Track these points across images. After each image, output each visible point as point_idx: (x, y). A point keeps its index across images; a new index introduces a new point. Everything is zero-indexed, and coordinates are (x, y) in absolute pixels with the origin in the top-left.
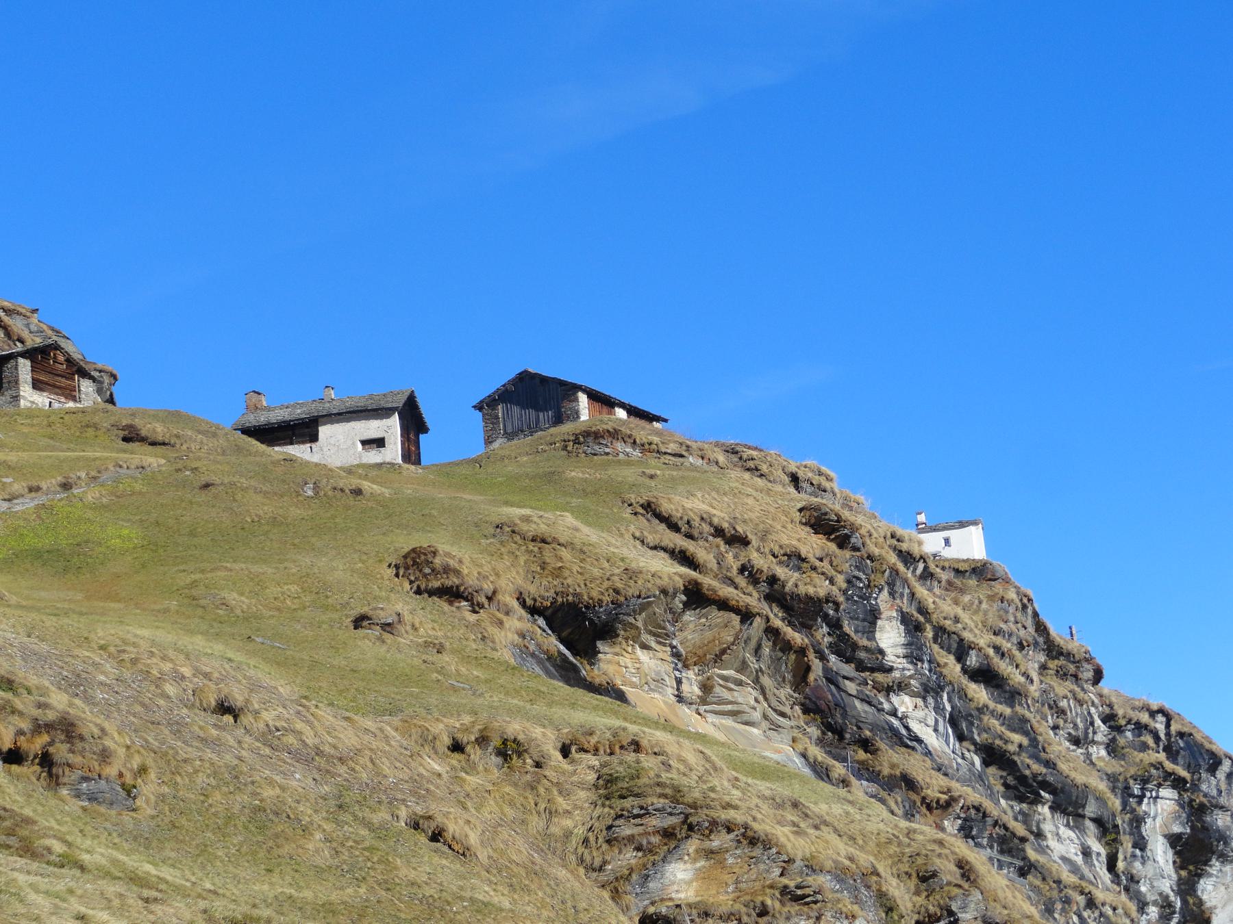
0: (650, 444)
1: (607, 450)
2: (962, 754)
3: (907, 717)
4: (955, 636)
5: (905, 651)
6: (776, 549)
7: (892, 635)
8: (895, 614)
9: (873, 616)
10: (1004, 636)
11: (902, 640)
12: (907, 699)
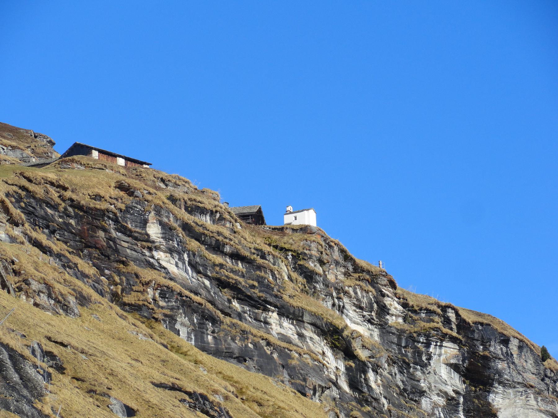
0: (88, 164)
1: (69, 166)
2: (198, 279)
3: (159, 259)
4: (214, 239)
5: (162, 236)
6: (91, 194)
7: (155, 229)
8: (155, 221)
9: (145, 222)
10: (63, 198)
11: (160, 231)
12: (161, 253)
